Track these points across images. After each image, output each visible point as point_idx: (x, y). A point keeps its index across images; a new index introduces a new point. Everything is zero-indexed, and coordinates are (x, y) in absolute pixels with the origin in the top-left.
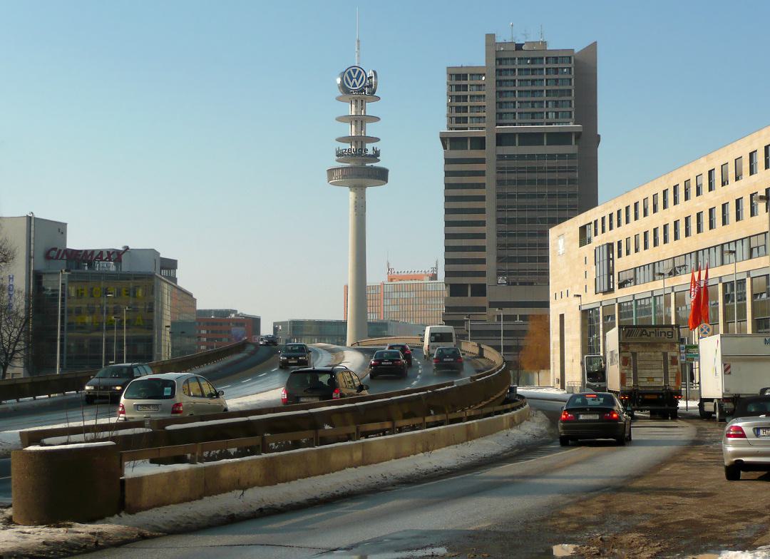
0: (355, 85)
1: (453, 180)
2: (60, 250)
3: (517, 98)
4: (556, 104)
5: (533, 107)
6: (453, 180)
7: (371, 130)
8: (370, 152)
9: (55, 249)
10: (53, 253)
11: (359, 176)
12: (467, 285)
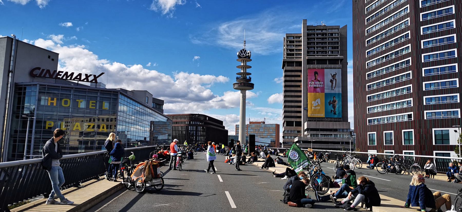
0: (243, 55)
1: (288, 79)
2: (43, 70)
3: (316, 45)
4: (333, 48)
5: (332, 40)
6: (288, 79)
7: (248, 71)
8: (248, 78)
9: (39, 68)
10: (37, 72)
11: (244, 86)
12: (293, 122)
